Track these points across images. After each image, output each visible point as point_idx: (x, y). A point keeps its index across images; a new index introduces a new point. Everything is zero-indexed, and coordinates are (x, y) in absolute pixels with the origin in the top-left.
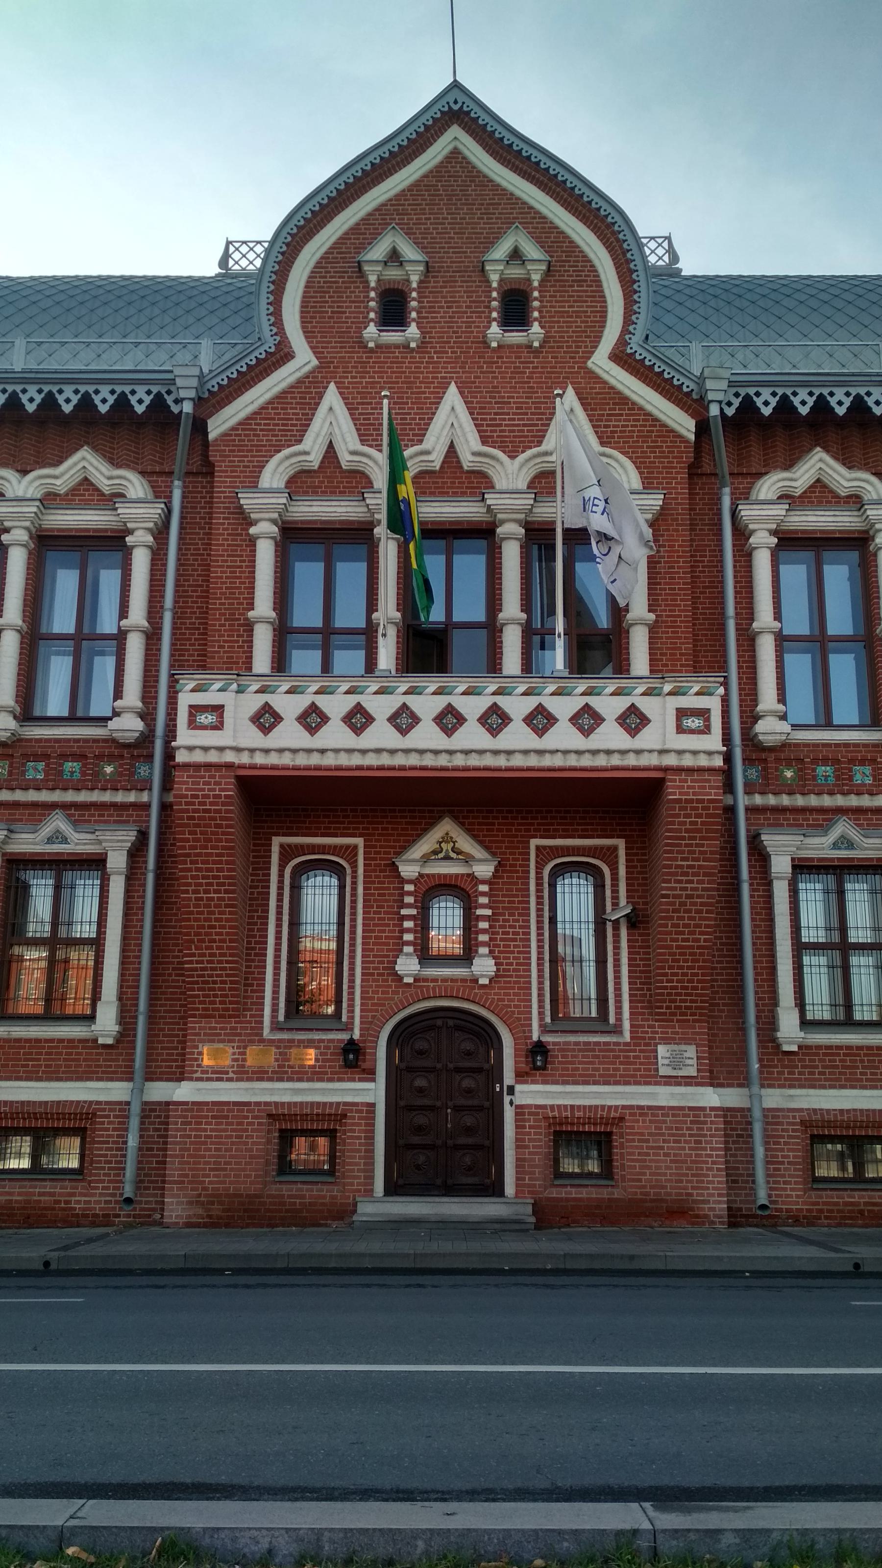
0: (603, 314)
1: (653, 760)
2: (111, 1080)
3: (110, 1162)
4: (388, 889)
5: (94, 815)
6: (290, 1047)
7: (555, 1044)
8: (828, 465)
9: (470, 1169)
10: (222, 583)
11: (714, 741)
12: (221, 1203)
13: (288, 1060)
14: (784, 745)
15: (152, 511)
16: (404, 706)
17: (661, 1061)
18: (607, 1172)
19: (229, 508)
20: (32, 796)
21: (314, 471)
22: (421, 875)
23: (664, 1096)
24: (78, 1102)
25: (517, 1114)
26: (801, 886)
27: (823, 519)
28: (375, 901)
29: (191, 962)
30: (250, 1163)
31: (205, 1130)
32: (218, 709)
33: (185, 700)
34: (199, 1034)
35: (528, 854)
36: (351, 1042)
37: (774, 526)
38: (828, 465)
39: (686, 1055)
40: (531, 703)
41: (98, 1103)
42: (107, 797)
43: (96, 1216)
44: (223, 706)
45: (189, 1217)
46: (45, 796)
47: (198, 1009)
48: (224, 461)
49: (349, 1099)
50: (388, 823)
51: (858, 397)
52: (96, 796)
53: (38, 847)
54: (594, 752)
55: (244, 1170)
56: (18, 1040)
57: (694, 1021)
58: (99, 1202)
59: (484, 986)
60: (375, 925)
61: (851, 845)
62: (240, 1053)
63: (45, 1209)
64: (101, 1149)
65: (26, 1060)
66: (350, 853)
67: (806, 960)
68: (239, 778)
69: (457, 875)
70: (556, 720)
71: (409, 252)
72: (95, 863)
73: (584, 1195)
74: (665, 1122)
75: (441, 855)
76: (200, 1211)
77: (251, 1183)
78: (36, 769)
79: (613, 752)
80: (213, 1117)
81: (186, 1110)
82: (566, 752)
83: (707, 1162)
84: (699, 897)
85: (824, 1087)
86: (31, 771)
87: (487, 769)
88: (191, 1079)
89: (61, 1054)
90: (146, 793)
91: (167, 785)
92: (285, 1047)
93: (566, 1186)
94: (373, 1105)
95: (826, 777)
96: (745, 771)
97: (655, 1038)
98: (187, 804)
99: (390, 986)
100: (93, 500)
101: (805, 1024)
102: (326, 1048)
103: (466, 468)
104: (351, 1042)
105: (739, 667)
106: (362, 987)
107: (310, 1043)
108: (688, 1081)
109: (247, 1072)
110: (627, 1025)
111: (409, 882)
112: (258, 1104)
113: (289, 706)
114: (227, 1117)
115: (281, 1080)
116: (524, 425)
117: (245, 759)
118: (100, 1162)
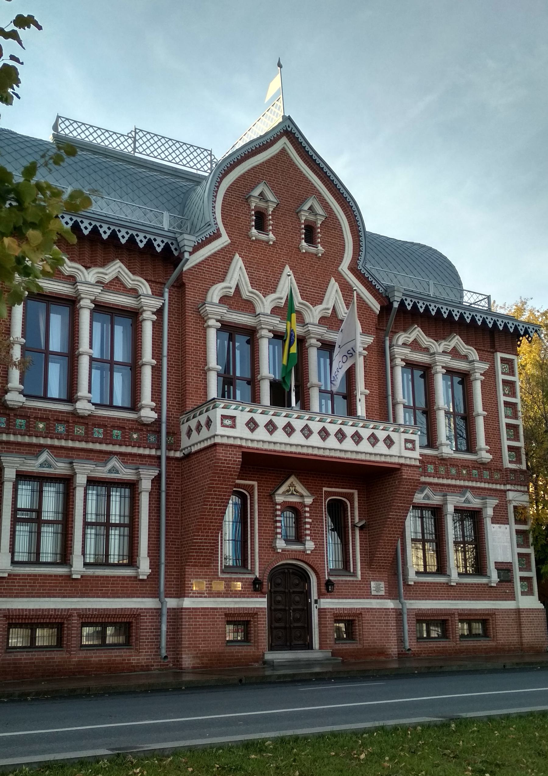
0: (344, 246)
1: (396, 460)
2: (144, 597)
3: (148, 639)
4: (268, 507)
5: (129, 460)
6: (231, 581)
8: (420, 334)
10: (192, 347)
12: (207, 657)
13: (230, 588)
14: (21, 407)
15: (158, 303)
16: (307, 426)
17: (372, 589)
18: (486, 634)
19: (193, 308)
21: (230, 297)
23: (374, 604)
24: (131, 609)
26: (20, 487)
27: (418, 357)
28: (263, 512)
29: (197, 539)
30: (218, 637)
31: (199, 622)
32: (233, 418)
34: (191, 575)
36: (256, 579)
37: (93, 298)
38: (420, 334)
39: (381, 586)
41: (141, 609)
43: (142, 666)
44: (235, 417)
45: (193, 664)
47: (191, 562)
48: (190, 283)
49: (258, 606)
50: (268, 475)
51: (132, 235)
53: (104, 474)
54: (376, 454)
55: (216, 640)
56: (97, 577)
57: (384, 571)
58: (144, 659)
60: (264, 524)
61: (50, 466)
62: (209, 584)
63: (118, 664)
64: (143, 632)
65: (102, 587)
66: (250, 489)
67: (18, 528)
69: (295, 502)
71: (270, 196)
73: (348, 647)
74: (376, 615)
75: (290, 493)
76: (198, 661)
77: (220, 646)
78: (99, 433)
79: (327, 449)
80: (202, 615)
81: (190, 612)
83: (390, 632)
85: (420, 600)
86: (96, 433)
88: (188, 597)
89: (119, 584)
92: (229, 581)
93: (124, 649)
95: (117, 436)
97: (369, 579)
98: (222, 463)
99: (271, 553)
100: (121, 290)
101: (86, 564)
102: (246, 582)
103: (244, 297)
106: (259, 553)
107: (238, 580)
109: (212, 593)
110: (359, 573)
112: (221, 608)
114: (208, 615)
115: (227, 597)
116: (315, 293)
118: (143, 639)
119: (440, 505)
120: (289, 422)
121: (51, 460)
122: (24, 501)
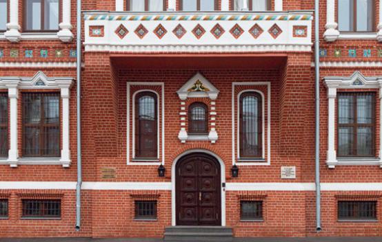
7: (241, 166)
9: (208, 215)
11: (308, 41)
16: (180, 26)
20: (28, 65)
22: (188, 98)
25: (226, 194)
26: (340, 100)
32: (101, 27)
33: (88, 23)
35: (231, 88)
36: (161, 166)
40: (233, 23)
42: (60, 65)
46: (33, 65)
52: (55, 65)
54: (259, 46)
59: (213, 144)
61: (361, 83)
66: (159, 88)
67: (340, 130)
68: (111, 58)
69: (202, 98)
70: (243, 31)
72: (56, 93)
82: (247, 46)
84: (300, 107)
87: (126, 53)
90: (75, 63)
91: (82, 61)
94: (170, 191)
96: (320, 52)
104: (161, 166)
105: (320, 6)
108: (292, 180)
111: (183, 101)
113: (131, 26)
117: (113, 50)
119: (376, 89)
120: (160, 25)
121: (362, 79)
122: (344, 113)
